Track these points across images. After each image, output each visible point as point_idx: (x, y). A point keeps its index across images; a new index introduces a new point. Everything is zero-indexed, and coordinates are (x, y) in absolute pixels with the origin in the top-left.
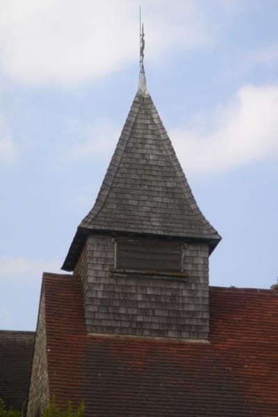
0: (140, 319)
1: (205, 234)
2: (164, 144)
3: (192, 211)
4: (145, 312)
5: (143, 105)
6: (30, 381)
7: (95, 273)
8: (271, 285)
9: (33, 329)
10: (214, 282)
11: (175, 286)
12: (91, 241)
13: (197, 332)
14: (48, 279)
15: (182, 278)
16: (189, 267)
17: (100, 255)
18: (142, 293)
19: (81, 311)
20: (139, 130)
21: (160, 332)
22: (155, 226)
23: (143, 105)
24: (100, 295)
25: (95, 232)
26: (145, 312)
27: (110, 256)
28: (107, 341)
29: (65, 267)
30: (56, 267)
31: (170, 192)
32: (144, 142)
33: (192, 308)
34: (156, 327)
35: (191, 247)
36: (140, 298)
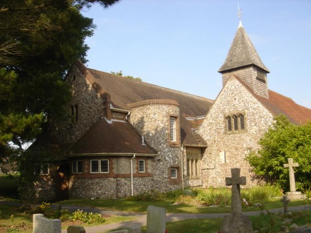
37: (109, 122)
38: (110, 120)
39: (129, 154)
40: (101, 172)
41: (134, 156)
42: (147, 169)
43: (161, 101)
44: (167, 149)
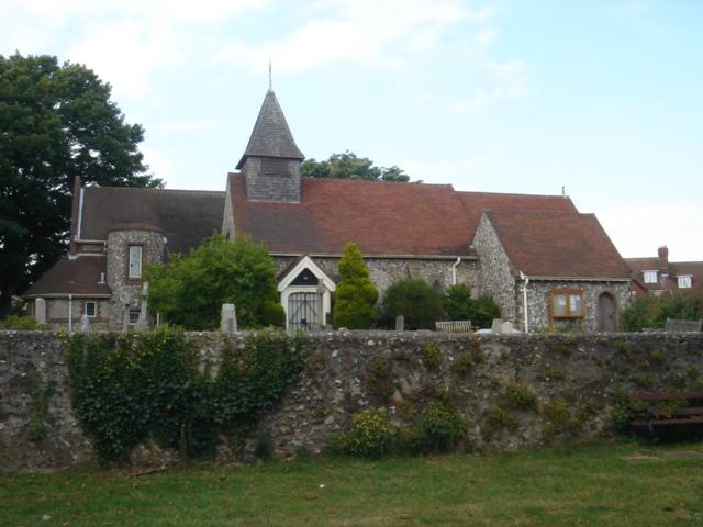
1: (298, 156)
2: (280, 115)
4: (273, 190)
5: (271, 96)
6: (507, 251)
7: (251, 175)
9: (224, 189)
12: (249, 159)
13: (295, 199)
17: (254, 167)
18: (271, 182)
19: (245, 193)
20: (269, 109)
21: (280, 199)
22: (277, 153)
23: (271, 96)
28: (257, 204)
29: (237, 168)
31: (283, 137)
32: (271, 114)
37: (71, 257)
38: (73, 255)
41: (459, 259)
42: (99, 312)
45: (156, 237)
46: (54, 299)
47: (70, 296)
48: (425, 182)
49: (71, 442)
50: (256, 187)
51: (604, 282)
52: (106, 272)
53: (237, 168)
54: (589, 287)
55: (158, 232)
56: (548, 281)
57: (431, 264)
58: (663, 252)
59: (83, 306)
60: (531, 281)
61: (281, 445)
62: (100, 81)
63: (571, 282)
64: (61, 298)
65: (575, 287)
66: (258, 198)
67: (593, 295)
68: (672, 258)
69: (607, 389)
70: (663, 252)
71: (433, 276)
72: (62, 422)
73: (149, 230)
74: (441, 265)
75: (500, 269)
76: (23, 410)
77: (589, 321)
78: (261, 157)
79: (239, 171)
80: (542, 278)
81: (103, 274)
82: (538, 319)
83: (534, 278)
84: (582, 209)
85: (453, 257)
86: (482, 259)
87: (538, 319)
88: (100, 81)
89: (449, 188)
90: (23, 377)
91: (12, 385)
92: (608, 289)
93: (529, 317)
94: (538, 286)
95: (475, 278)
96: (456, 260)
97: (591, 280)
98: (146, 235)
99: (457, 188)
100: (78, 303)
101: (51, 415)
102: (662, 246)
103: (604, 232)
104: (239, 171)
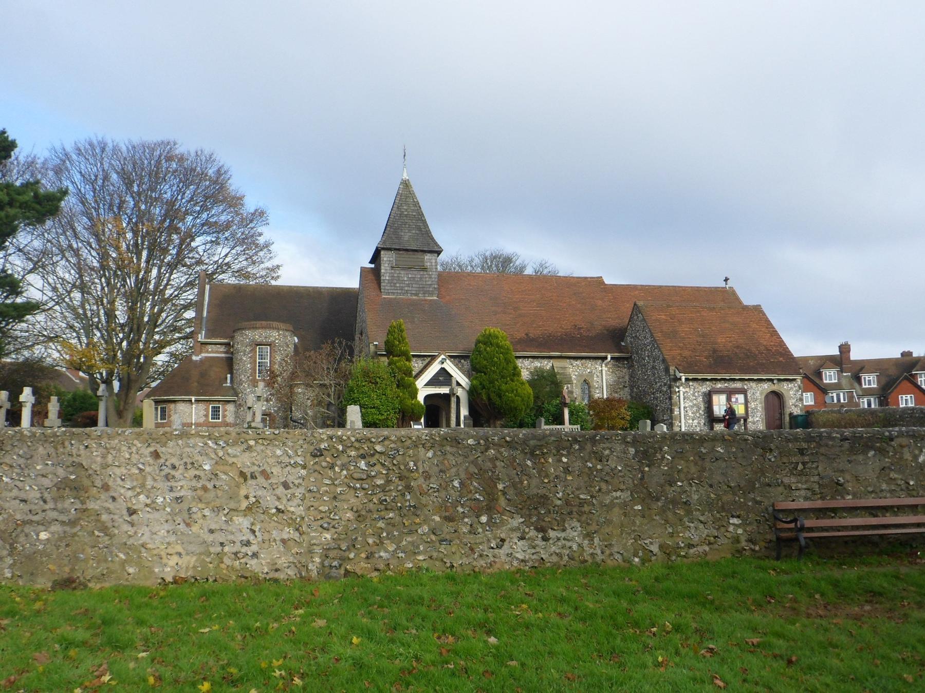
0: (406, 288)
2: (417, 204)
3: (841, 564)
4: (408, 285)
5: (406, 184)
8: (136, 140)
10: (852, 358)
11: (422, 273)
13: (431, 294)
14: (363, 271)
15: (425, 269)
16: (428, 264)
18: (405, 276)
21: (416, 295)
23: (406, 184)
24: (387, 278)
25: (384, 249)
26: (408, 285)
27: (391, 259)
29: (370, 262)
30: (915, 355)
33: (430, 283)
34: (414, 292)
35: (429, 255)
36: (406, 279)
39: (187, 398)
40: (159, 421)
41: (683, 379)
42: (224, 416)
43: (258, 323)
44: (248, 390)
45: (285, 336)
46: (174, 401)
47: (193, 399)
48: (561, 274)
49: (127, 554)
50: (390, 282)
51: (772, 380)
52: (232, 373)
53: (370, 262)
54: (753, 384)
55: (287, 330)
56: (706, 380)
57: (578, 362)
58: (845, 349)
59: (207, 410)
60: (687, 380)
61: (367, 558)
62: (523, 268)
63: (716, 380)
64: (184, 401)
65: (738, 385)
66: (393, 293)
67: (758, 394)
68: (855, 355)
69: (752, 496)
70: (845, 349)
71: (580, 375)
72: (116, 532)
73: (278, 329)
74: (589, 363)
75: (654, 367)
76: (71, 517)
77: (754, 423)
78: (395, 249)
79: (373, 266)
80: (700, 376)
81: (229, 376)
82: (696, 421)
83: (691, 376)
84: (747, 300)
85: (603, 354)
86: (635, 356)
87: (696, 421)
88: (523, 268)
89: (599, 281)
90: (71, 480)
91: (59, 489)
92: (775, 387)
93: (685, 418)
94: (695, 384)
95: (627, 378)
96: (606, 358)
97: (755, 378)
98: (275, 334)
99: (608, 281)
100: (202, 406)
101: (104, 523)
102: (843, 341)
103: (684, 289)
104: (373, 266)
